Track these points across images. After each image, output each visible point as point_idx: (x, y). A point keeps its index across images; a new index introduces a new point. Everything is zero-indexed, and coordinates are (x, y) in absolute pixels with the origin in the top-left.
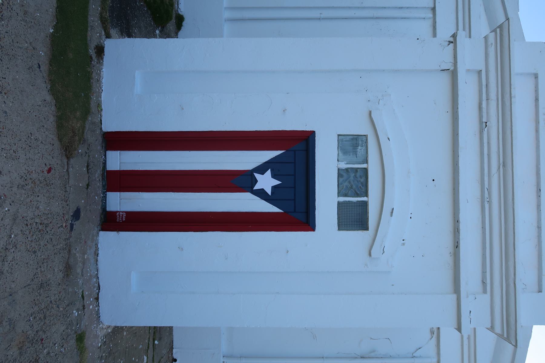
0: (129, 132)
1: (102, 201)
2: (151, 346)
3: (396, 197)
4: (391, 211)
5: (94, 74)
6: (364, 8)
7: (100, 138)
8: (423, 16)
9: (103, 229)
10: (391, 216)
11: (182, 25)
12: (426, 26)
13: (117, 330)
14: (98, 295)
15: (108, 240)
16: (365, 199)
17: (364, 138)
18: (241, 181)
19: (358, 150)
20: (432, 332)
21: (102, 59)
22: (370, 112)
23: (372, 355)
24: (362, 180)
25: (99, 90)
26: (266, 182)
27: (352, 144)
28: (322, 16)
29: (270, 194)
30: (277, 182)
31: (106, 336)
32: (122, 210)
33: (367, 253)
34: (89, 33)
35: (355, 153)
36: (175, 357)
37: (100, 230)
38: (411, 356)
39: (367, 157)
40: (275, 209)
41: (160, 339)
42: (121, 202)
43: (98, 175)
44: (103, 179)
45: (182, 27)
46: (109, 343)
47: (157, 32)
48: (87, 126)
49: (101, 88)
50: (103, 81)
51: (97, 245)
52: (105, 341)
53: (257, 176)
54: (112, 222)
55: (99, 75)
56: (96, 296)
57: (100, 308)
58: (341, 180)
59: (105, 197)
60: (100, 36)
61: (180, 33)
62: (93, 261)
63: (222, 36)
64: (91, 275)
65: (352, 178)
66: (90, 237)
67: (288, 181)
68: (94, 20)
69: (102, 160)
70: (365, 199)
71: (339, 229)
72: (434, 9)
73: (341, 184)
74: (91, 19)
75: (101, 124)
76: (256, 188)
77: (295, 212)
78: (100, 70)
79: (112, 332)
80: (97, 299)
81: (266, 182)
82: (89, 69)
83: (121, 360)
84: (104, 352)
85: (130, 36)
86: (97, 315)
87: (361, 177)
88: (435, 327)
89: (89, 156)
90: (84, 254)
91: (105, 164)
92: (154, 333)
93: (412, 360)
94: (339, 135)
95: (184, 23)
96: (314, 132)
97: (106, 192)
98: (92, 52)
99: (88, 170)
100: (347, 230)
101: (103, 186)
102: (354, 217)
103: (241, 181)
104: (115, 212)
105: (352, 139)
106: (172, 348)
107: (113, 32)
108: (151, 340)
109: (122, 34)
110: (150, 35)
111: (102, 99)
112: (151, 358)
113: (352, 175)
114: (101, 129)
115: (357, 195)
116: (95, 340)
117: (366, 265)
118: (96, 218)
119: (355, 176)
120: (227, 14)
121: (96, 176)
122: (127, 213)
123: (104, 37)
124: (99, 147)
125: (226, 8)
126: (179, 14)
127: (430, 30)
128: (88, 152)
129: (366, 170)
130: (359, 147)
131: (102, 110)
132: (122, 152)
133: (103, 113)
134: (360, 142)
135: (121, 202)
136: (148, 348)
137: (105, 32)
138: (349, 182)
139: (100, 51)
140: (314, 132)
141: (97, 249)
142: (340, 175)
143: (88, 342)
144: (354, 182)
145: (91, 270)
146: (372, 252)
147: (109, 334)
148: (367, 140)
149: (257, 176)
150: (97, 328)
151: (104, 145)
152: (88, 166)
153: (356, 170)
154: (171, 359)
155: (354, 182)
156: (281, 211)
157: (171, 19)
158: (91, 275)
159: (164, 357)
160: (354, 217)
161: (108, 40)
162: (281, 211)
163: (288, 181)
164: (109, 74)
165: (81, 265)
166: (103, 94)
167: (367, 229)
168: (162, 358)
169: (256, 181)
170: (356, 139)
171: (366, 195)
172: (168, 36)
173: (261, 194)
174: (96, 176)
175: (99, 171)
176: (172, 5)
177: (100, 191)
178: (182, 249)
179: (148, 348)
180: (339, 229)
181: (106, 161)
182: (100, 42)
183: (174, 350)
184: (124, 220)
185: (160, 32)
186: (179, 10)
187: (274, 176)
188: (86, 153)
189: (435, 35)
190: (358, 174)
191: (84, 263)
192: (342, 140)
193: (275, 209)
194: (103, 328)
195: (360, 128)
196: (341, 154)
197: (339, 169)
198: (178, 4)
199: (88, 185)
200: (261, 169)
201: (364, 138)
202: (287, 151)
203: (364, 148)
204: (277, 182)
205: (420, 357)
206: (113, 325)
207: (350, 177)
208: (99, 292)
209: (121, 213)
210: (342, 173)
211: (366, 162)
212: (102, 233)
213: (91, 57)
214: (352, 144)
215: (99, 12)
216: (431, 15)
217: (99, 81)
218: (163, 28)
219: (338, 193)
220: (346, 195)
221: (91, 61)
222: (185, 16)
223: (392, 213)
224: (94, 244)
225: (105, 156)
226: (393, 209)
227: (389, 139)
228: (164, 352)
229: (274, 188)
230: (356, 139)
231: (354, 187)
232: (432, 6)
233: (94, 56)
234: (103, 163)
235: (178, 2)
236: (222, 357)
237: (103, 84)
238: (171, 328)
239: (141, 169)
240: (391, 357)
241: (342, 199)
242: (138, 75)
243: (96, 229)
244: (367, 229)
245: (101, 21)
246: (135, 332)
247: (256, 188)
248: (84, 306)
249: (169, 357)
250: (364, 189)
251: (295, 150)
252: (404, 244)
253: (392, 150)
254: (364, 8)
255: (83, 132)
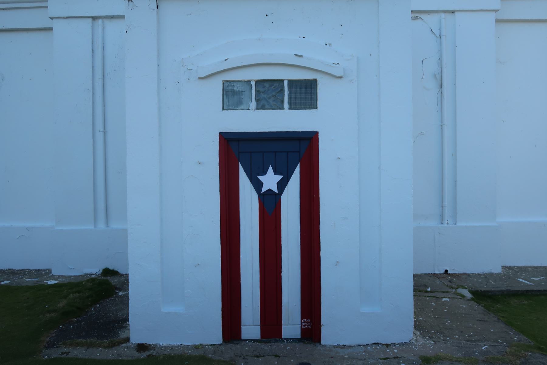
0: (222, 317)
1: (291, 342)
2: (433, 294)
3: (284, 53)
4: (297, 57)
5: (166, 353)
6: (93, 88)
7: (229, 345)
8: (100, 29)
9: (319, 340)
10: (302, 56)
11: (113, 270)
12: (112, 27)
13: (417, 326)
14: (383, 344)
15: (329, 335)
16: (286, 83)
17: (226, 84)
18: (270, 206)
19: (237, 89)
20: (416, 18)
21: (150, 345)
22: (200, 78)
23: (438, 77)
24: (267, 85)
25: (182, 347)
26: (270, 180)
27: (232, 96)
28: (102, 130)
29: (282, 177)
30: (271, 169)
31: (423, 336)
32: (300, 323)
33: (339, 81)
34: (125, 358)
35: (240, 93)
36: (443, 272)
37: (320, 344)
38: (439, 38)
39: (244, 81)
40: (297, 171)
41: (426, 286)
42: (292, 323)
43: (266, 347)
44: (270, 342)
45: (115, 269)
46: (431, 333)
47: (120, 293)
48: (218, 358)
49: (179, 346)
50: (172, 343)
51: (334, 347)
52: (429, 337)
53: (264, 189)
54: (312, 331)
55: (166, 348)
56: (385, 346)
57: (397, 342)
58: (267, 107)
59: (287, 340)
60: (127, 348)
61: (121, 271)
62: (350, 350)
63: (125, 230)
64: (365, 352)
65: (265, 96)
66: (327, 353)
67: (269, 159)
68: (111, 354)
69: (251, 343)
70: (286, 83)
71: (316, 108)
72: (94, 18)
73: (271, 106)
74: (110, 357)
75: (215, 345)
76: (276, 190)
77: (300, 152)
78: (161, 347)
79: (420, 331)
80: (387, 345)
81: (270, 180)
82: (161, 357)
83: (447, 322)
84: (439, 338)
85: (126, 320)
86: (403, 345)
87: (264, 87)
88: (411, 15)
89: (247, 356)
90: (344, 358)
91: (254, 341)
92: (420, 291)
93: (443, 38)
94: (223, 109)
95: (111, 268)
96: (220, 133)
97: (282, 339)
98: (144, 355)
99: (261, 357)
100: (317, 100)
101: (276, 341)
102: (304, 93)
103: (270, 206)
104: (302, 329)
105: (227, 95)
106: (434, 275)
107: (123, 336)
108: (427, 294)
109: (125, 327)
110: (126, 298)
111: (190, 344)
112: (444, 294)
113: (262, 95)
114: (220, 345)
115: (282, 90)
116: (427, 346)
117: (351, 81)
118: (309, 347)
119: (263, 93)
120: (101, 225)
121: (266, 348)
122: (302, 318)
123: (128, 344)
124: (238, 346)
125: (95, 227)
126: (102, 273)
127: (115, 22)
128: (243, 357)
129: (258, 82)
130: (235, 88)
131: (201, 345)
132: (242, 323)
133: (204, 343)
134: (230, 88)
135: (292, 323)
136: (434, 297)
137: (123, 343)
138: (269, 98)
139: (142, 347)
140: (220, 133)
141: (339, 346)
142: (263, 108)
143: (430, 353)
144: (269, 93)
145: (359, 352)
146: (338, 75)
147: (421, 334)
148: (227, 81)
149: (264, 189)
150: (416, 345)
151: (235, 342)
152: (257, 357)
153: (257, 92)
154: (445, 276)
155: (269, 93)
156: (299, 165)
157: (107, 280)
158: (365, 352)
159: (444, 282)
160: (304, 93)
161: (131, 340)
162: (299, 165)
163: (269, 159)
164: (164, 338)
165: (354, 361)
166: (186, 344)
167: (315, 81)
168: (444, 284)
169: (270, 190)
170: (227, 92)
171: (282, 81)
172: (127, 282)
173: (282, 185)
174: (266, 348)
175: (262, 346)
176: (93, 280)
177: (282, 345)
178: (337, 262)
179: (434, 297)
180: (316, 108)
181: (252, 340)
182: (133, 348)
183: (436, 273)
184: (309, 321)
185: (120, 291)
186: (98, 273)
187: (264, 173)
188: (244, 358)
189: (123, 17)
190: (262, 89)
191: (353, 358)
192: (228, 106)
193: (297, 171)
194: (416, 340)
195: (216, 88)
196: (242, 107)
197: (257, 109)
198: (92, 275)
199: (276, 356)
200: (258, 185)
201: (226, 84)
202: (239, 160)
203: (235, 84)
204: (271, 169)
205: (440, 30)
206: (412, 329)
207: (265, 98)
208: (381, 344)
209: (303, 324)
210: (260, 106)
211: (249, 81)
212: (323, 342)
213: (149, 356)
214: (232, 96)
215: (103, 350)
216: (100, 21)
217: (172, 348)
218: (116, 289)
219: (280, 109)
220: (283, 102)
221: (153, 356)
222: (104, 268)
223: (299, 56)
224: (334, 349)
225: (246, 340)
226: (296, 55)
227: (226, 60)
228: (438, 282)
229: (276, 172)
230: (227, 92)
231: (274, 93)
232: (90, 20)
233: (148, 353)
234: (254, 342)
235: (90, 275)
236: (442, 225)
237: (176, 343)
238: (415, 276)
239: (259, 305)
240: (440, 59)
241: (286, 105)
242: (166, 309)
243: (318, 348)
244: (315, 81)
245: (112, 347)
246: (419, 310)
247: (276, 190)
248: (395, 358)
249: (443, 277)
250: (276, 84)
251: (238, 152)
252: (330, 44)
253: (237, 57)
254: (93, 88)
255: (224, 362)
